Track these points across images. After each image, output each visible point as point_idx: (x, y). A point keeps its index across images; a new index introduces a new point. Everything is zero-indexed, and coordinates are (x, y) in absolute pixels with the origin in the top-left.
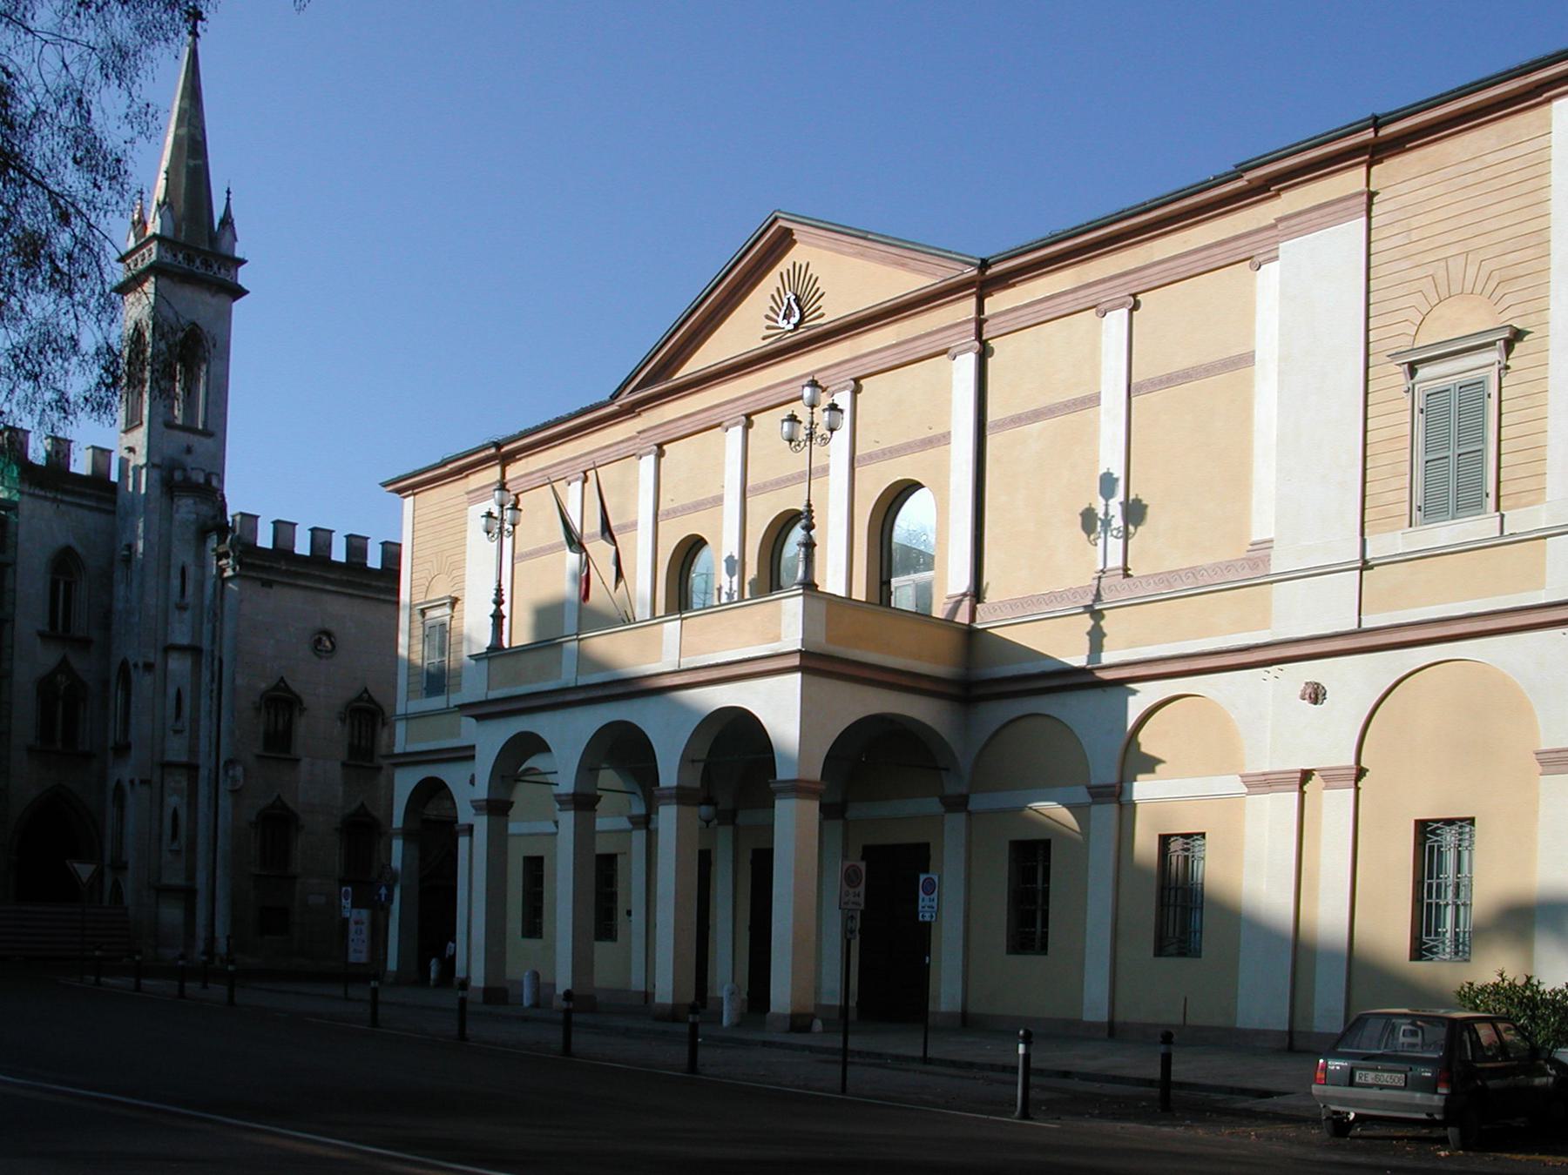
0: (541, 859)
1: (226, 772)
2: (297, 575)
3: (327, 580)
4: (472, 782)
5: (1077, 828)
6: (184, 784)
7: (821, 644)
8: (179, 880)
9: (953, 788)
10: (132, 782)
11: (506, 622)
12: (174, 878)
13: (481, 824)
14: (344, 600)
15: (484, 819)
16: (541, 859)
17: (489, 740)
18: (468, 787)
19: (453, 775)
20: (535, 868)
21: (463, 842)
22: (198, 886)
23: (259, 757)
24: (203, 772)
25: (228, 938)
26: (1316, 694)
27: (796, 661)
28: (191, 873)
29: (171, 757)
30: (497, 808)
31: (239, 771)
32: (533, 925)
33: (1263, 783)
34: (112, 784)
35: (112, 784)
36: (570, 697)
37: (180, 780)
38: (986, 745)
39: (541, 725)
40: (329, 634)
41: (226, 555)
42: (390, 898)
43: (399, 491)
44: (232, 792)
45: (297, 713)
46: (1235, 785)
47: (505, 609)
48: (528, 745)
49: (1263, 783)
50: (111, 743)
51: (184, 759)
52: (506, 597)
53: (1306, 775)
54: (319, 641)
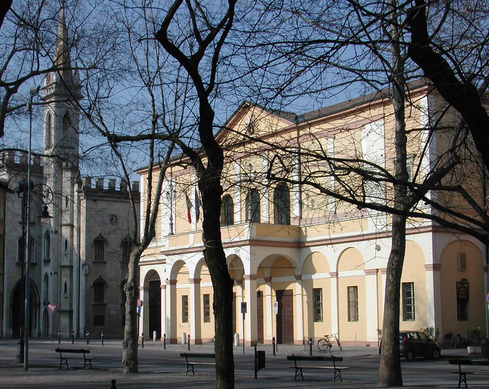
0: (187, 296)
1: (83, 268)
2: (104, 197)
3: (114, 197)
4: (165, 271)
5: (287, 289)
6: (69, 273)
7: (255, 237)
8: (67, 308)
9: (298, 273)
10: (51, 273)
11: (173, 225)
12: (65, 307)
13: (168, 287)
14: (120, 203)
15: (169, 286)
16: (187, 296)
17: (171, 260)
18: (164, 276)
19: (158, 268)
20: (185, 299)
21: (163, 291)
22: (73, 309)
23: (93, 262)
24: (75, 268)
25: (84, 328)
26: (378, 248)
27: (248, 242)
28: (71, 305)
29: (63, 264)
30: (173, 282)
31: (87, 267)
32: (185, 319)
33: (369, 272)
34: (43, 274)
35: (43, 274)
36: (191, 250)
37: (67, 272)
38: (305, 261)
39: (184, 258)
40: (116, 216)
41: (81, 192)
42: (139, 311)
43: (138, 173)
44: (85, 275)
45: (105, 246)
46: (362, 273)
47: (173, 221)
48: (179, 264)
49: (369, 272)
50: (43, 259)
51: (68, 264)
52: (174, 218)
53: (378, 270)
54: (112, 218)
